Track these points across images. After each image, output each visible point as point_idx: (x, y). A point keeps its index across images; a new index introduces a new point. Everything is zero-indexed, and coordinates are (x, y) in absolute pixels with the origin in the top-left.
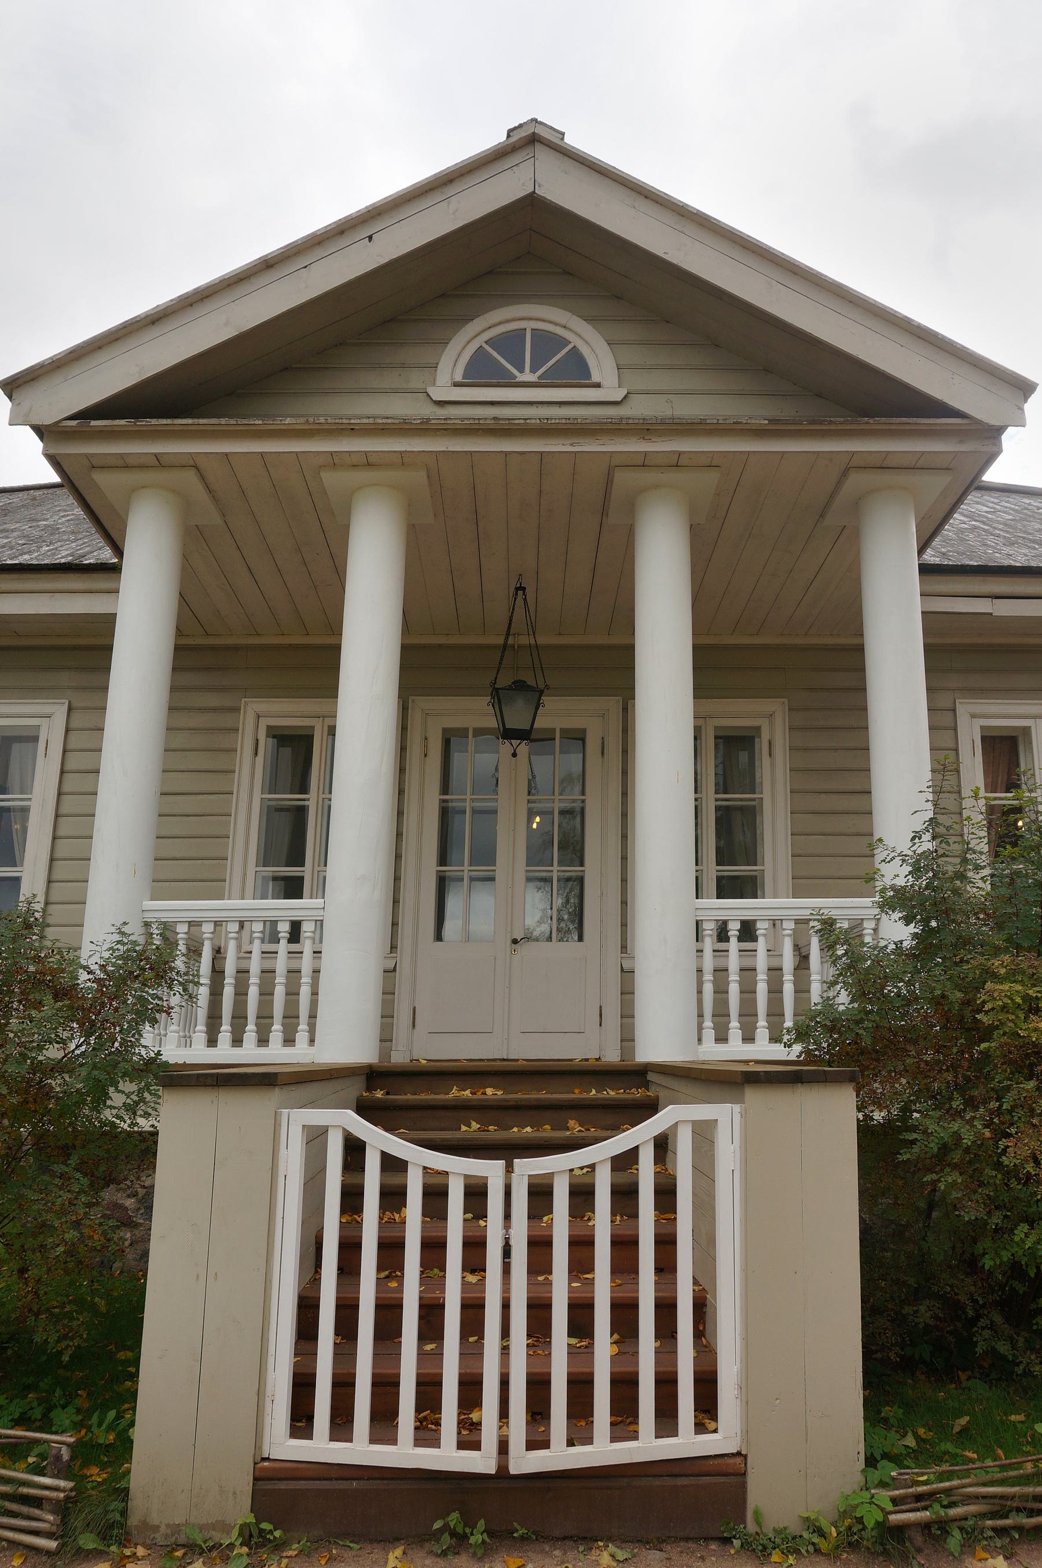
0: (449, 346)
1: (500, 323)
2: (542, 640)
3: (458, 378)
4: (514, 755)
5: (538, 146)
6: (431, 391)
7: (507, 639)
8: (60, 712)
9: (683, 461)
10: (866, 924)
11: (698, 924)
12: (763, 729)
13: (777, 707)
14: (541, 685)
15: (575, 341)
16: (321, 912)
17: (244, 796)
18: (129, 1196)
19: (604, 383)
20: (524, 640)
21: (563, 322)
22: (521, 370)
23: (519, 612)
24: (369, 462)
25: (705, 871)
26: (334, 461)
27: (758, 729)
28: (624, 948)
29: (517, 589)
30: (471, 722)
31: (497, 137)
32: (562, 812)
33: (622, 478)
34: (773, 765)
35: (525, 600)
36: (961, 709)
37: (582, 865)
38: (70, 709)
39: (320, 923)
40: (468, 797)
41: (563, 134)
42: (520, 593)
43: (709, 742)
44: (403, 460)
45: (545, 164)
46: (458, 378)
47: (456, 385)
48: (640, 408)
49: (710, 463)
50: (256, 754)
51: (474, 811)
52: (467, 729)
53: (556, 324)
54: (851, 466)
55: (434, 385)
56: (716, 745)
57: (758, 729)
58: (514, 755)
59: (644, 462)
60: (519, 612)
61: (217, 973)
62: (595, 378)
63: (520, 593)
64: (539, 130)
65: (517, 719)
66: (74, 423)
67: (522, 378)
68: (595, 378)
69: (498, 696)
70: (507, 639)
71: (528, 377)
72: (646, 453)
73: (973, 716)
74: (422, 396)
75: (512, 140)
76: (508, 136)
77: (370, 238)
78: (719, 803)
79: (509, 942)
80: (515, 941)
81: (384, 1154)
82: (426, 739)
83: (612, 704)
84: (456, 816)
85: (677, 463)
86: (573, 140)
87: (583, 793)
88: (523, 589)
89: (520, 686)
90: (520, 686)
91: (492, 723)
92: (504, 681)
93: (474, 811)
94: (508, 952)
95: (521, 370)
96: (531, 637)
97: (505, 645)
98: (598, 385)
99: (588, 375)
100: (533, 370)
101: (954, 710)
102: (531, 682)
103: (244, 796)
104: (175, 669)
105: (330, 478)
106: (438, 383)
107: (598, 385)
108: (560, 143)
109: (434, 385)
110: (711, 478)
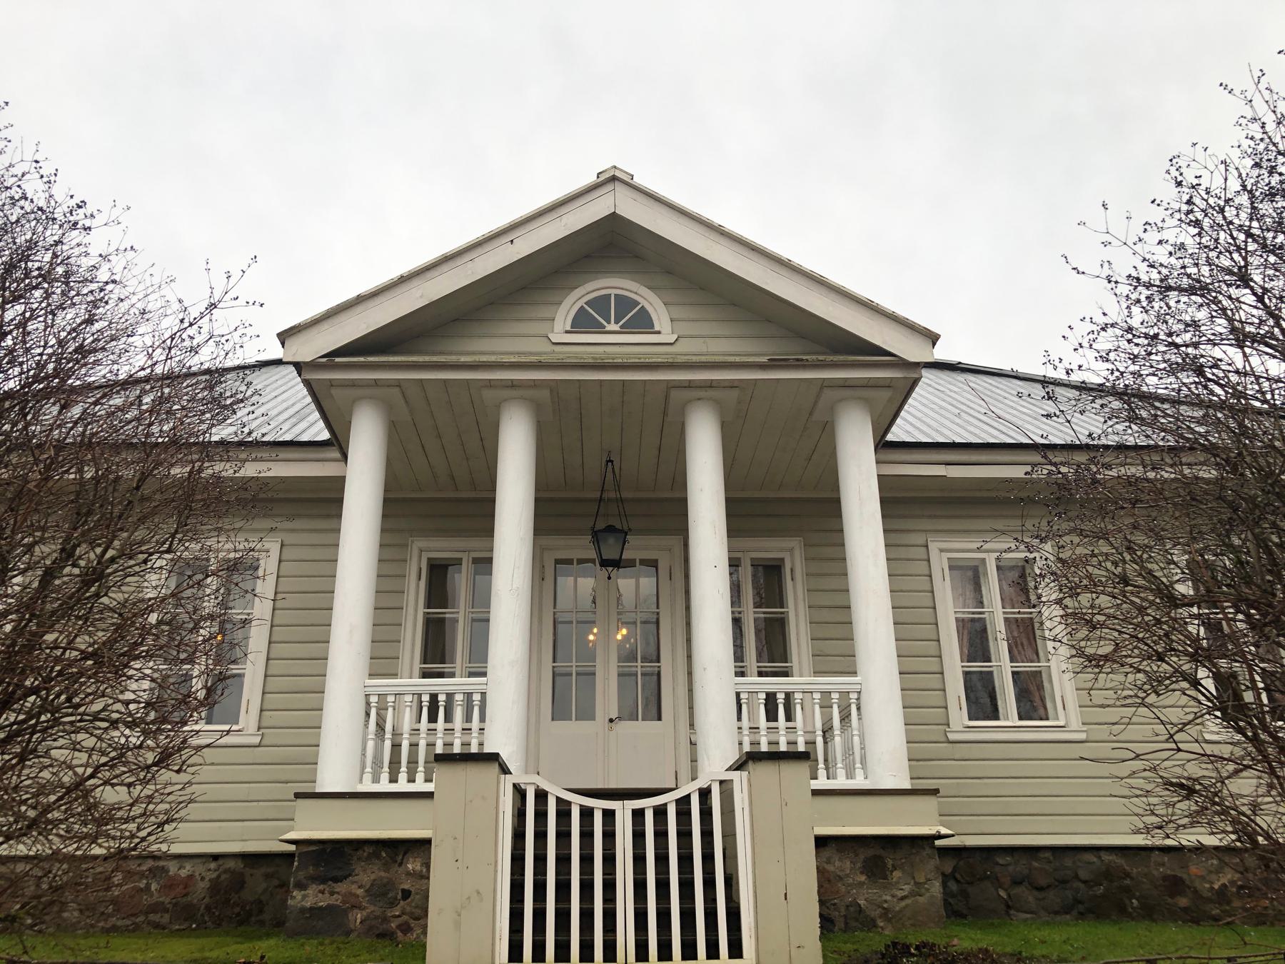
0: (562, 305)
1: (594, 291)
2: (625, 494)
3: (568, 328)
4: (609, 578)
5: (617, 183)
6: (550, 336)
7: (602, 494)
8: (274, 548)
9: (714, 384)
10: (852, 696)
11: (738, 694)
12: (786, 560)
13: (795, 543)
14: (626, 528)
15: (643, 303)
16: (485, 687)
17: (411, 610)
18: (359, 887)
19: (663, 331)
20: (612, 495)
21: (635, 291)
22: (609, 322)
23: (610, 476)
24: (513, 385)
25: (749, 666)
26: (490, 384)
27: (782, 560)
28: (692, 725)
29: (608, 462)
30: (576, 554)
31: (591, 179)
32: (642, 623)
33: (674, 394)
34: (794, 587)
35: (613, 468)
36: (934, 547)
37: (659, 662)
38: (282, 545)
39: (483, 694)
40: (574, 664)
41: (633, 176)
42: (610, 464)
43: (746, 573)
44: (535, 384)
45: (622, 195)
46: (568, 328)
47: (567, 332)
48: (688, 349)
49: (732, 385)
50: (420, 579)
51: (578, 622)
52: (573, 560)
53: (631, 291)
54: (825, 384)
55: (553, 331)
56: (754, 576)
57: (782, 560)
58: (609, 578)
59: (690, 385)
60: (610, 476)
61: (396, 747)
62: (657, 328)
63: (610, 464)
64: (618, 174)
65: (610, 553)
66: (325, 360)
67: (610, 327)
68: (657, 328)
69: (597, 536)
70: (602, 494)
71: (616, 327)
72: (690, 381)
73: (942, 551)
74: (546, 339)
75: (600, 180)
76: (598, 177)
77: (512, 241)
78: (757, 615)
79: (607, 720)
80: (611, 721)
81: (557, 798)
82: (543, 567)
83: (675, 541)
84: (634, 580)
85: (710, 385)
86: (638, 180)
87: (658, 608)
88: (612, 462)
89: (610, 529)
90: (610, 529)
91: (592, 554)
92: (601, 525)
93: (578, 674)
94: (607, 729)
95: (609, 322)
96: (618, 493)
97: (601, 499)
98: (659, 332)
99: (652, 326)
100: (616, 322)
101: (927, 546)
102: (619, 526)
103: (411, 610)
104: (385, 516)
105: (488, 394)
106: (555, 331)
107: (659, 332)
108: (630, 181)
109: (553, 331)
110: (734, 394)
